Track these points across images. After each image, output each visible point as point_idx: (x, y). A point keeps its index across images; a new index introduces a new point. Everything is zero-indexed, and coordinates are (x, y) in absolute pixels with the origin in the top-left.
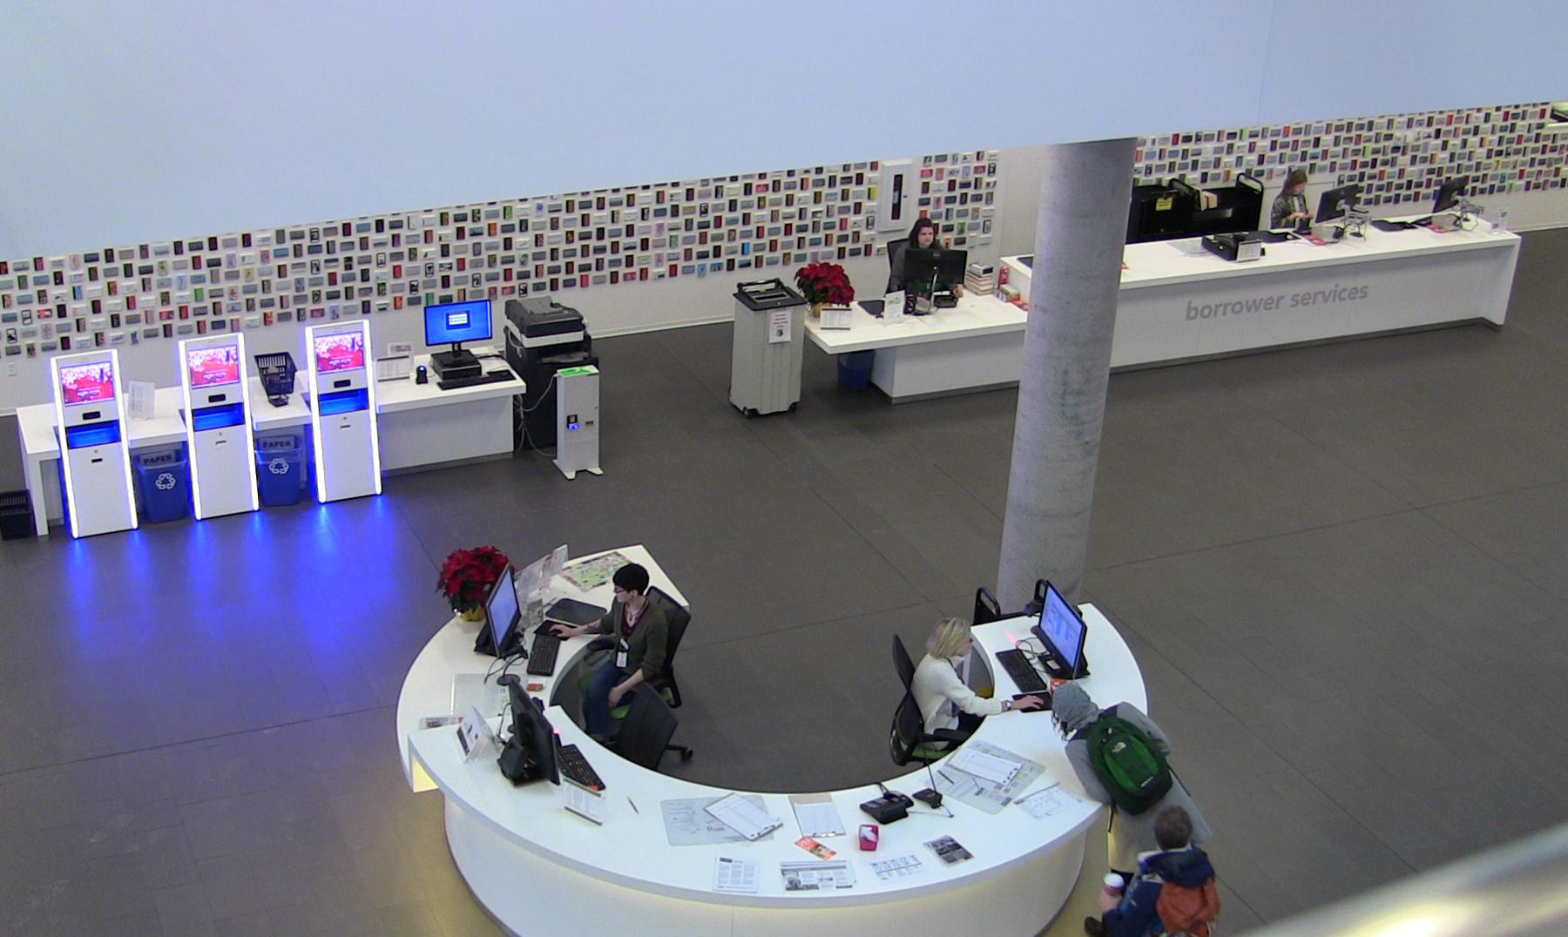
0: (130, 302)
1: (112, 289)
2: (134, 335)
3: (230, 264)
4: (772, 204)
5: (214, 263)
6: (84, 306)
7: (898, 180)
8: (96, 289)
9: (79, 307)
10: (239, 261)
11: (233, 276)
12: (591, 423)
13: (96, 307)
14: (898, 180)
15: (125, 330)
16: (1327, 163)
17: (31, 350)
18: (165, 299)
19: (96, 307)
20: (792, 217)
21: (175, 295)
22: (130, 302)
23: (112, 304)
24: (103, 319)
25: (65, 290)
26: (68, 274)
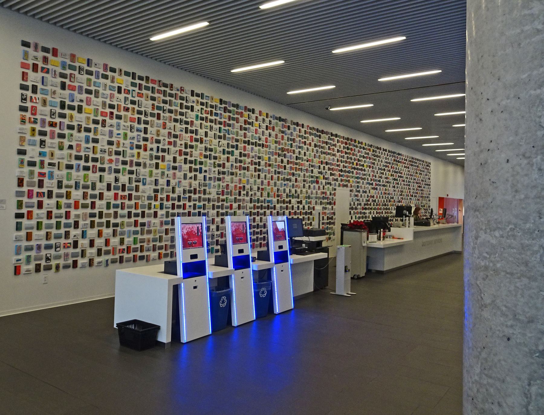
0: (107, 242)
1: (100, 234)
2: (107, 261)
3: (149, 225)
4: (128, 207)
5: (143, 225)
6: (86, 242)
7: (319, 213)
8: (92, 233)
9: (84, 243)
10: (152, 225)
11: (149, 232)
12: (448, 195)
13: (92, 243)
14: (319, 213)
15: (103, 258)
16: (131, 255)
17: (57, 267)
18: (122, 242)
19: (92, 243)
20: (32, 228)
21: (126, 240)
22: (107, 242)
23: (99, 242)
24: (94, 250)
25: (79, 232)
26: (81, 223)
